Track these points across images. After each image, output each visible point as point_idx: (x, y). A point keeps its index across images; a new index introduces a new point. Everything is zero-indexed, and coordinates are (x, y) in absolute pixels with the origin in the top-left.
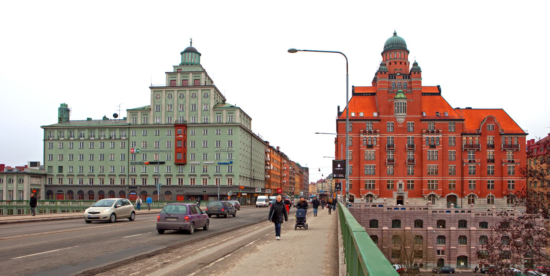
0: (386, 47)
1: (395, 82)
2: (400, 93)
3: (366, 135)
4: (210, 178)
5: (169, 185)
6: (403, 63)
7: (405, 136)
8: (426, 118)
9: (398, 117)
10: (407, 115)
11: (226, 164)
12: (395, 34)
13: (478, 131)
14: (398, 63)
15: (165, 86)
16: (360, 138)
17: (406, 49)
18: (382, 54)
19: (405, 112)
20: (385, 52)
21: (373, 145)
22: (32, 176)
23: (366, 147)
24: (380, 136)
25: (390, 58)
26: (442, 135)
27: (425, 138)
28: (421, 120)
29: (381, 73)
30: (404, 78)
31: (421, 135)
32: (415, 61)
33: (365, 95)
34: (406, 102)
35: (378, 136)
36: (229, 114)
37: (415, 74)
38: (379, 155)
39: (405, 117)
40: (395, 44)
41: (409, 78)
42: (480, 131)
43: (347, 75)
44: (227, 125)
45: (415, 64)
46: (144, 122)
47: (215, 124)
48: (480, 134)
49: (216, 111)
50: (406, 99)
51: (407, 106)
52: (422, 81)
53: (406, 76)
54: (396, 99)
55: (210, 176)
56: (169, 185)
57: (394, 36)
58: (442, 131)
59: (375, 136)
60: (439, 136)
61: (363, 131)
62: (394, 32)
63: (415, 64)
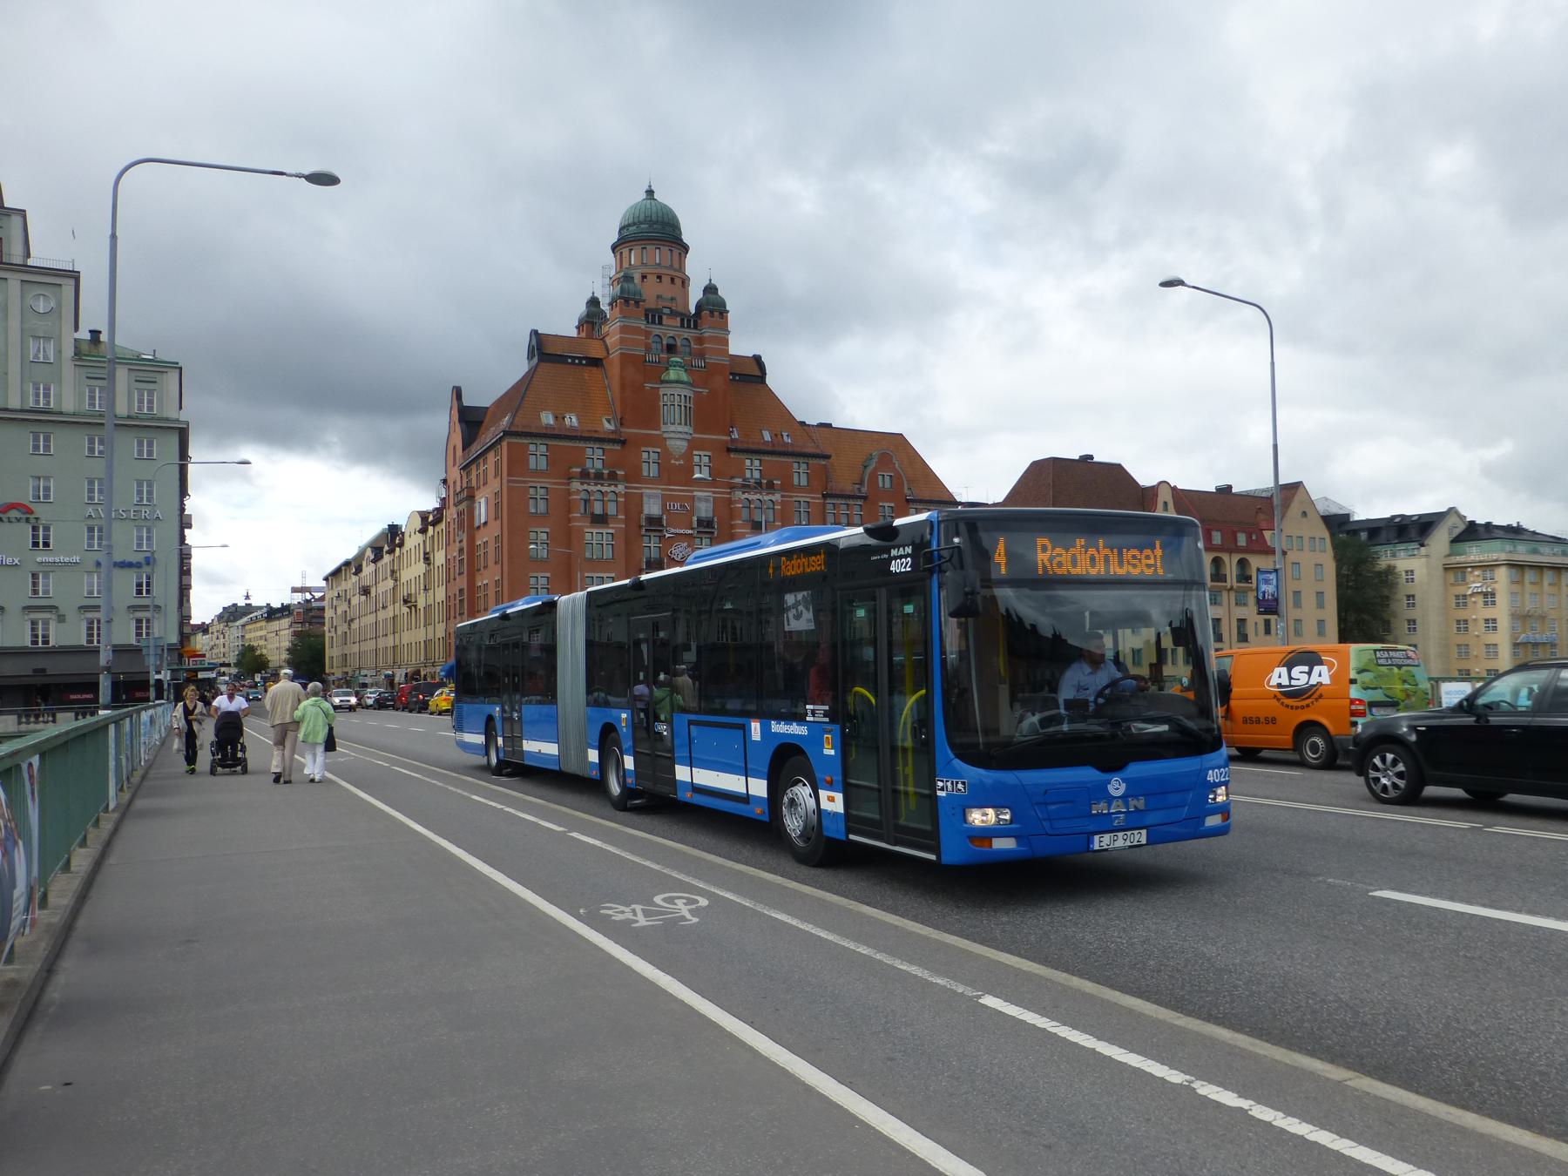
0: (631, 229)
1: (661, 334)
2: (675, 366)
3: (589, 484)
4: (61, 619)
5: (40, 645)
6: (678, 281)
7: (688, 491)
8: (740, 446)
9: (672, 435)
10: (695, 431)
11: (130, 565)
12: (650, 192)
13: (859, 489)
14: (666, 280)
15: (21, 263)
16: (569, 493)
17: (681, 240)
18: (614, 248)
19: (683, 423)
20: (621, 244)
21: (607, 514)
22: (1542, 653)
23: (589, 519)
24: (626, 487)
25: (630, 262)
26: (782, 496)
27: (578, 492)
28: (729, 450)
29: (627, 301)
30: (682, 326)
31: (569, 484)
32: (710, 280)
33: (573, 363)
34: (692, 396)
35: (621, 488)
36: (137, 383)
37: (638, 307)
38: (623, 546)
39: (689, 437)
40: (656, 222)
41: (696, 327)
42: (864, 490)
43: (1273, 364)
44: (132, 425)
45: (710, 289)
46: (140, 408)
47: (84, 416)
48: (865, 498)
49: (85, 370)
50: (692, 385)
51: (692, 406)
52: (731, 338)
53: (689, 321)
54: (667, 382)
55: (62, 611)
56: (40, 645)
57: (647, 199)
58: (626, 475)
59: (613, 488)
60: (773, 498)
61: (579, 470)
62: (646, 188)
63: (710, 289)
